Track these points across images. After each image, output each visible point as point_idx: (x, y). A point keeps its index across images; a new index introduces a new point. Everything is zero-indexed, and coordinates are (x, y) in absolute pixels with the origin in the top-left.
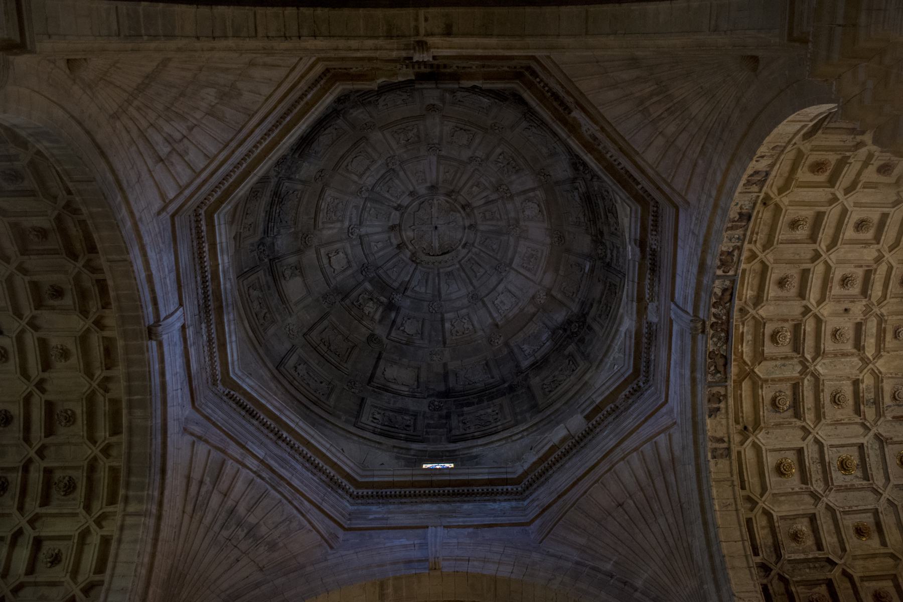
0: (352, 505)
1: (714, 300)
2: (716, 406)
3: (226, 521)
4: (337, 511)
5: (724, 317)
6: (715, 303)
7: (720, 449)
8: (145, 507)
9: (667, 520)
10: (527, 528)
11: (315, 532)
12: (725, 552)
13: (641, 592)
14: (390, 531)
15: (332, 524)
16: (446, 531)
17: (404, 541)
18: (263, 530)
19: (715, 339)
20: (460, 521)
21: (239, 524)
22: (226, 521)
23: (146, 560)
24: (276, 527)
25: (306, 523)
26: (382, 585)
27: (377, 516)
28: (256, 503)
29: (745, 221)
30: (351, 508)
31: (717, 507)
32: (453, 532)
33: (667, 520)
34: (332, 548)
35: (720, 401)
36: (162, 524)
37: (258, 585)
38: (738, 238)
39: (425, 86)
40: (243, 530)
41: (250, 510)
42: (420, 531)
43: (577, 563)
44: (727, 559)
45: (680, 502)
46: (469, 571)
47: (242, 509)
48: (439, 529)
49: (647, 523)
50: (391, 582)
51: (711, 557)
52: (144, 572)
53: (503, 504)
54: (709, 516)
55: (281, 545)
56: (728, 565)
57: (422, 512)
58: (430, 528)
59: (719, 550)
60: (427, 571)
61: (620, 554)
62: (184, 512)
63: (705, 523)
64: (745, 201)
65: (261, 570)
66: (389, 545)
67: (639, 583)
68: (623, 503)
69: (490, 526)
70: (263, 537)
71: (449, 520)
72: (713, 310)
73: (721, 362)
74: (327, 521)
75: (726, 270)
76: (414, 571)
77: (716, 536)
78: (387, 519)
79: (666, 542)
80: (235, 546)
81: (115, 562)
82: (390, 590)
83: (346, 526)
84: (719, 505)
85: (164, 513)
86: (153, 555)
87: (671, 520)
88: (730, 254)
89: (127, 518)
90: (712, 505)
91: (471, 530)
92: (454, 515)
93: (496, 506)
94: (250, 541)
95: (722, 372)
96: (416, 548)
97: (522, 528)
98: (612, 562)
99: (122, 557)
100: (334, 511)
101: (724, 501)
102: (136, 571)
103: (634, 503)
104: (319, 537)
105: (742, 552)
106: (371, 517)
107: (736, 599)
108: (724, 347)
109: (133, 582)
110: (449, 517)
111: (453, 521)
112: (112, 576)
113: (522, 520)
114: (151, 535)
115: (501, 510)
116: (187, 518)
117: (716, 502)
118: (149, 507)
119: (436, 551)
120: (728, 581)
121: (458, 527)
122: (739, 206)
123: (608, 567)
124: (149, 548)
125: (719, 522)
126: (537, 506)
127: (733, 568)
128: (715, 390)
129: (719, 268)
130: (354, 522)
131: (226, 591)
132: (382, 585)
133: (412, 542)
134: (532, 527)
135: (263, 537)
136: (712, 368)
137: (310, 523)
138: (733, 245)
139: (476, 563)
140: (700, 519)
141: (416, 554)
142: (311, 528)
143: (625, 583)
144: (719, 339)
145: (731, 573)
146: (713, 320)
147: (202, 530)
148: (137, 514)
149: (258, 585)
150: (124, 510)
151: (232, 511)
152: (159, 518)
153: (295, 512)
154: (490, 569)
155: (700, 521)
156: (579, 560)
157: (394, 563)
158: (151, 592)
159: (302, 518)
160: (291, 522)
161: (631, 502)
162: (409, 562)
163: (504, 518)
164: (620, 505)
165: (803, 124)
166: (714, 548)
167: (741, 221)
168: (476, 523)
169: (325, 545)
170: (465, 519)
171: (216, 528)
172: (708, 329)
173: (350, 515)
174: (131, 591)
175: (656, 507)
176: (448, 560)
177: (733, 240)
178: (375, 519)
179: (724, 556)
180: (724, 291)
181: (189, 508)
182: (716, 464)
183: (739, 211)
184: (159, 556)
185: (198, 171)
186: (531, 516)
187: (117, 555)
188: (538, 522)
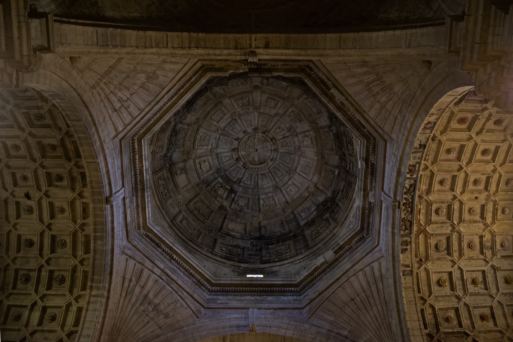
4: (201, 298)
5: (410, 200)
6: (406, 192)
10: (302, 311)
11: (189, 309)
12: (409, 326)
15: (198, 305)
17: (236, 316)
18: (162, 307)
19: (405, 212)
24: (169, 305)
29: (423, 148)
30: (208, 297)
31: (405, 302)
32: (262, 311)
34: (198, 318)
35: (407, 245)
36: (110, 301)
40: (151, 307)
41: (155, 296)
42: (245, 310)
43: (329, 330)
44: (410, 330)
45: (385, 298)
47: (151, 296)
50: (229, 337)
51: (401, 329)
53: (289, 297)
55: (171, 315)
56: (411, 334)
57: (246, 300)
59: (406, 325)
61: (352, 326)
62: (121, 296)
63: (398, 311)
65: (160, 328)
71: (260, 305)
72: (405, 196)
73: (408, 224)
74: (196, 303)
77: (404, 317)
78: (227, 303)
79: (377, 320)
81: (84, 321)
83: (206, 307)
85: (111, 296)
86: (104, 318)
87: (380, 309)
88: (414, 166)
89: (91, 298)
90: (402, 301)
91: (272, 311)
92: (263, 302)
93: (285, 298)
98: (347, 330)
99: (88, 318)
104: (191, 312)
105: (418, 327)
106: (219, 302)
108: (410, 216)
109: (93, 332)
112: (82, 328)
114: (104, 307)
115: (288, 301)
116: (122, 298)
117: (404, 299)
121: (265, 309)
122: (420, 140)
123: (345, 333)
124: (102, 314)
125: (406, 310)
126: (308, 299)
127: (413, 335)
128: (405, 239)
130: (209, 304)
131: (142, 338)
134: (305, 310)
136: (404, 227)
137: (187, 304)
139: (274, 329)
141: (242, 323)
144: (408, 212)
146: (405, 201)
147: (130, 306)
151: (146, 296)
152: (108, 298)
153: (179, 298)
154: (282, 332)
155: (396, 309)
156: (330, 328)
157: (231, 327)
159: (183, 301)
160: (177, 303)
161: (358, 298)
162: (238, 327)
164: (352, 300)
166: (403, 324)
169: (194, 316)
170: (270, 305)
171: (137, 305)
172: (402, 206)
173: (208, 300)
176: (260, 326)
177: (416, 159)
178: (221, 303)
179: (408, 329)
180: (411, 186)
181: (124, 294)
182: (405, 279)
183: (419, 143)
184: (107, 318)
186: (304, 304)
187: (85, 317)
188: (308, 308)
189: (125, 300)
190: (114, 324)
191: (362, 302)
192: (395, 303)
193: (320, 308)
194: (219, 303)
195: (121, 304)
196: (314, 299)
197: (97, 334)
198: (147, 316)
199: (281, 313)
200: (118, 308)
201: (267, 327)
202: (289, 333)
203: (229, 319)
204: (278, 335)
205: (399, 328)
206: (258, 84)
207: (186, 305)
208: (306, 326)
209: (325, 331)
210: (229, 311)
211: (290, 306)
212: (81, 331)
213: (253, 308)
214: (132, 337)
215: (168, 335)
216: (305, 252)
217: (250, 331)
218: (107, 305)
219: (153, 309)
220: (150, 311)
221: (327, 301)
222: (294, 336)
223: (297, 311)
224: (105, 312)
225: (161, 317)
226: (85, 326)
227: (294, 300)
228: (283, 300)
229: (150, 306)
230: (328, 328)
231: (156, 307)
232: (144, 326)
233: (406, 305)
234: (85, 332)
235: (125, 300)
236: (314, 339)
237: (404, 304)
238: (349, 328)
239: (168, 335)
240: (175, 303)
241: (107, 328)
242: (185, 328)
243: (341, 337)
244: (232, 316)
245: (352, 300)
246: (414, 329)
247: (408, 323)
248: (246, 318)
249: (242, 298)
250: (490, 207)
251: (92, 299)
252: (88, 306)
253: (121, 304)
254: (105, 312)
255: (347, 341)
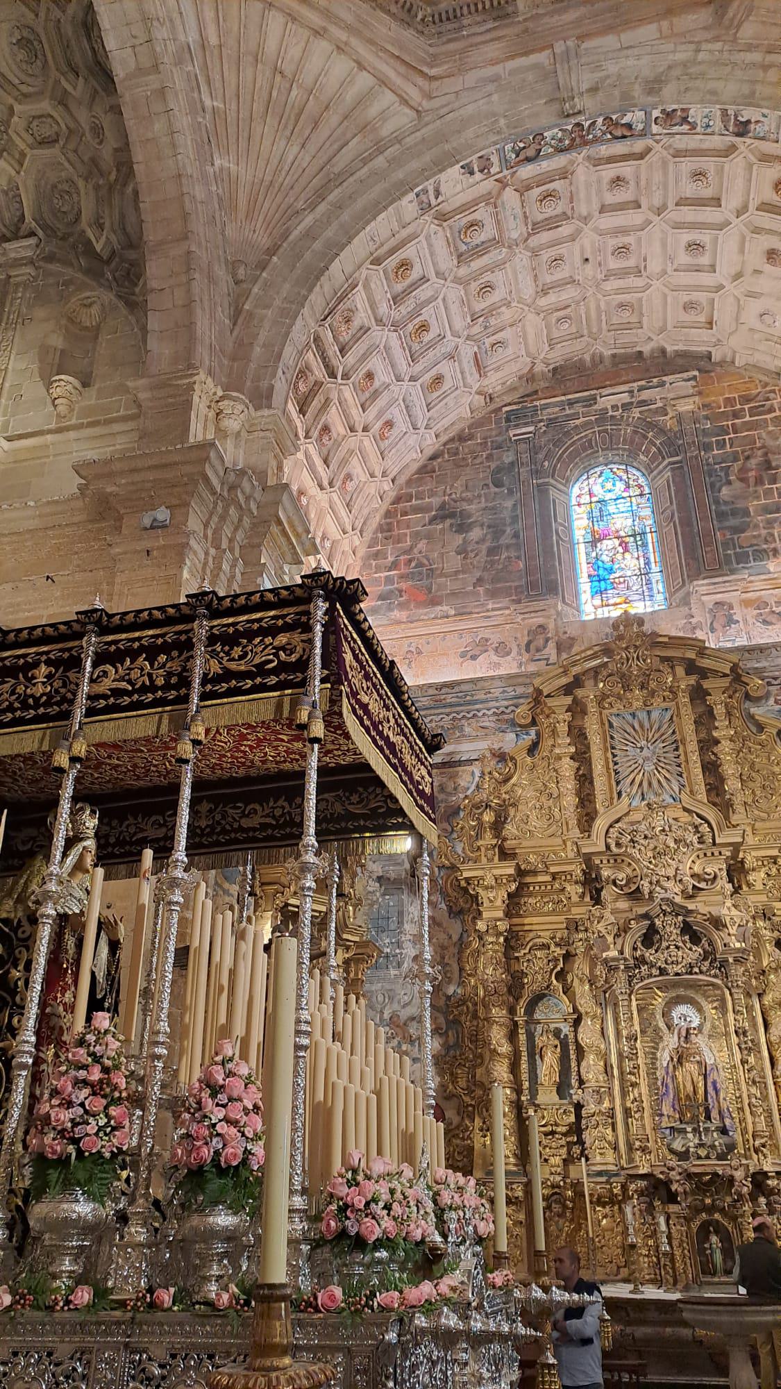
1: (614, 117)
2: (476, 169)
5: (591, 136)
6: (611, 119)
7: (428, 198)
19: (560, 135)
29: (736, 130)
35: (481, 171)
38: (708, 126)
64: (770, 125)
72: (600, 120)
73: (530, 152)
75: (659, 121)
84: (370, 231)
88: (685, 120)
95: (518, 159)
105: (337, 286)
108: (551, 150)
122: (762, 119)
128: (495, 159)
129: (663, 111)
136: (522, 145)
138: (699, 122)
144: (561, 140)
146: (586, 124)
165: (640, 793)
167: (736, 125)
172: (573, 121)
177: (706, 120)
180: (629, 126)
182: (411, 202)
183: (753, 120)
185: (675, 31)
250: (569, 293)
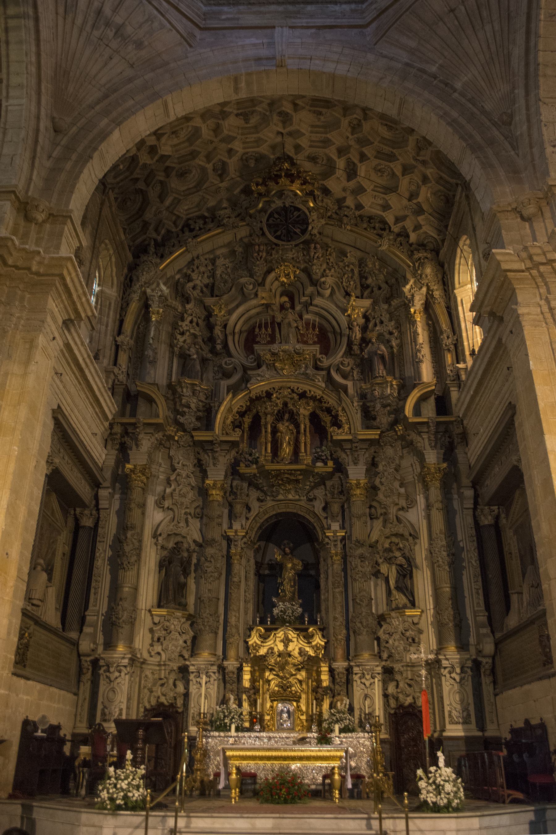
0: (205, 5)
3: (96, 21)
4: (193, 11)
8: (22, 9)
9: (493, 27)
10: (364, 30)
11: (174, 31)
12: (540, 60)
13: (459, 94)
14: (241, 30)
15: (189, 24)
16: (291, 32)
17: (254, 40)
18: (129, 30)
20: (304, 22)
21: (108, 24)
22: (96, 21)
23: (34, 59)
24: (140, 27)
25: (166, 22)
26: (236, 80)
27: (229, 16)
28: (119, 4)
30: (204, 9)
31: (542, 17)
32: (297, 32)
33: (493, 27)
34: (191, 46)
36: (41, 25)
37: (130, 80)
39: (548, 806)
40: (111, 31)
41: (115, 10)
42: (268, 31)
43: (407, 64)
44: (541, 67)
45: (509, 10)
46: (311, 69)
47: (107, 11)
48: (285, 29)
49: (474, 30)
50: (243, 78)
51: (527, 64)
52: (33, 69)
53: (344, 6)
54: (533, 25)
55: (146, 43)
56: (541, 73)
57: (269, 12)
58: (277, 28)
59: (536, 58)
60: (275, 68)
61: (445, 58)
62: (57, 14)
63: (528, 33)
65: (132, 66)
66: (240, 43)
67: (458, 85)
68: (455, 9)
69: (331, 27)
70: (130, 36)
71: (294, 20)
74: (184, 20)
76: (263, 68)
77: (536, 45)
78: (238, 19)
79: (489, 48)
80: (107, 45)
81: (8, 62)
82: (243, 85)
83: (202, 26)
85: (40, 15)
86: (38, 54)
87: (497, 27)
89: (9, 21)
90: (538, 15)
91: (313, 31)
92: (298, 16)
93: (337, 8)
94: (119, 40)
96: (265, 46)
97: (360, 30)
98: (437, 65)
99: (13, 57)
100: (191, 12)
101: (550, 11)
102: (27, 68)
103: (466, 9)
104: (179, 36)
106: (224, 17)
107: (541, 103)
109: (27, 78)
110: (294, 18)
111: (298, 22)
112: (8, 74)
113: (360, 22)
114: (33, 36)
115: (341, 13)
116: (60, 20)
117: (542, 12)
118: (26, 10)
119: (282, 50)
120: (537, 87)
121: (302, 27)
123: (434, 69)
124: (34, 49)
125: (542, 31)
126: (375, 9)
127: (545, 76)
130: (208, 22)
131: (105, 85)
132: (236, 80)
133: (261, 41)
134: (368, 29)
135: (130, 36)
137: (170, 23)
139: (317, 62)
140: (524, 28)
141: (264, 52)
142: (171, 28)
143: (447, 85)
145: (541, 80)
147: (76, 31)
148: (17, 17)
149: (130, 80)
150: (5, 13)
151: (99, 12)
152: (37, 20)
153: (156, 12)
154: (330, 67)
155: (524, 30)
156: (409, 61)
157: (246, 60)
158: (43, 87)
159: (162, 18)
160: (153, 22)
161: (463, 8)
162: (258, 60)
163: (344, 20)
164: (452, 10)
166: (531, 57)
168: (318, 24)
169: (185, 43)
170: (309, 20)
171: (88, 28)
173: (204, 15)
174: (27, 86)
175: (485, 14)
176: (293, 58)
178: (228, 19)
179: (538, 65)
181: (61, 10)
184: (43, 55)
186: (369, 19)
187: (8, 55)
188: (374, 25)
189: (65, 21)
190: (56, 63)
191: (468, 15)
192: (524, 19)
193: (395, 25)
194: (224, 20)
195: (60, 29)
196: (387, 9)
197: (34, 81)
198: (108, 48)
199: (329, 35)
200: (57, 35)
201: (305, 58)
202: (342, 69)
203: (243, 46)
204: (324, 73)
205: (523, 63)
206: (289, 111)
207: (168, 25)
208: (370, 57)
209: (400, 65)
210: (243, 32)
211: (344, 21)
212: (8, 79)
213: (282, 27)
214: (90, 83)
215: (146, 77)
216: (299, 777)
217: (277, 66)
218: (37, 31)
219: (116, 33)
220: (110, 38)
221: (408, 13)
222: (349, 74)
223: (355, 31)
224: (38, 45)
225: (130, 47)
226: (12, 69)
227: (352, 11)
228: (333, 11)
229: (109, 31)
230: (406, 60)
231: (119, 30)
232: (106, 64)
233: (542, 22)
234: (14, 80)
235: (65, 21)
236: (381, 79)
237: (540, 20)
238: (441, 62)
239: (146, 77)
240: (150, 22)
241: (47, 71)
242: (172, 65)
243: (425, 76)
244: (247, 41)
245: (452, 10)
246: (547, 66)
247: (541, 53)
248: (271, 44)
249: (262, 9)
251: (12, 23)
252: (7, 37)
253: (60, 29)
254: (38, 45)
255: (435, 82)
